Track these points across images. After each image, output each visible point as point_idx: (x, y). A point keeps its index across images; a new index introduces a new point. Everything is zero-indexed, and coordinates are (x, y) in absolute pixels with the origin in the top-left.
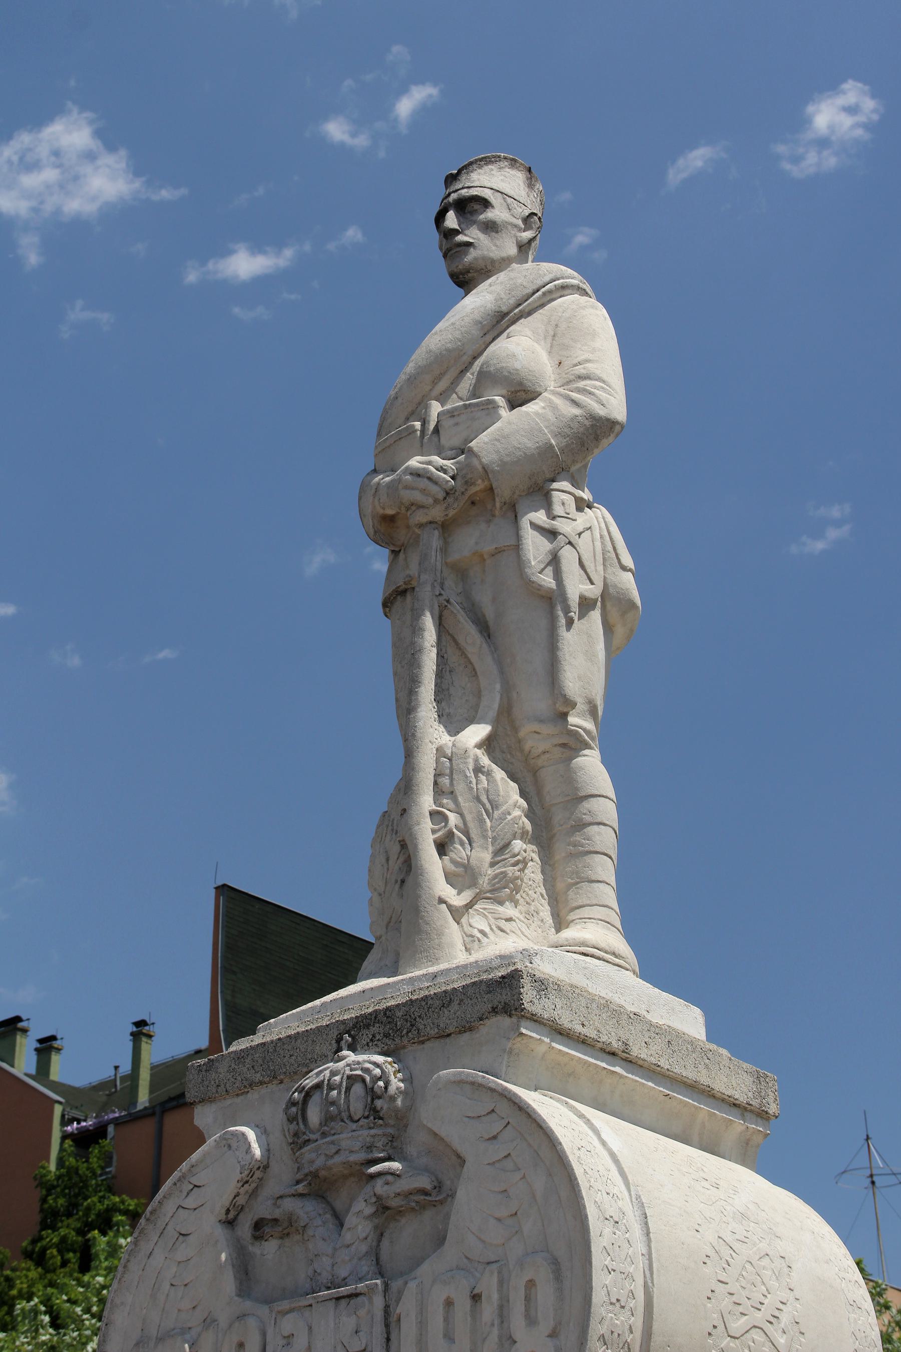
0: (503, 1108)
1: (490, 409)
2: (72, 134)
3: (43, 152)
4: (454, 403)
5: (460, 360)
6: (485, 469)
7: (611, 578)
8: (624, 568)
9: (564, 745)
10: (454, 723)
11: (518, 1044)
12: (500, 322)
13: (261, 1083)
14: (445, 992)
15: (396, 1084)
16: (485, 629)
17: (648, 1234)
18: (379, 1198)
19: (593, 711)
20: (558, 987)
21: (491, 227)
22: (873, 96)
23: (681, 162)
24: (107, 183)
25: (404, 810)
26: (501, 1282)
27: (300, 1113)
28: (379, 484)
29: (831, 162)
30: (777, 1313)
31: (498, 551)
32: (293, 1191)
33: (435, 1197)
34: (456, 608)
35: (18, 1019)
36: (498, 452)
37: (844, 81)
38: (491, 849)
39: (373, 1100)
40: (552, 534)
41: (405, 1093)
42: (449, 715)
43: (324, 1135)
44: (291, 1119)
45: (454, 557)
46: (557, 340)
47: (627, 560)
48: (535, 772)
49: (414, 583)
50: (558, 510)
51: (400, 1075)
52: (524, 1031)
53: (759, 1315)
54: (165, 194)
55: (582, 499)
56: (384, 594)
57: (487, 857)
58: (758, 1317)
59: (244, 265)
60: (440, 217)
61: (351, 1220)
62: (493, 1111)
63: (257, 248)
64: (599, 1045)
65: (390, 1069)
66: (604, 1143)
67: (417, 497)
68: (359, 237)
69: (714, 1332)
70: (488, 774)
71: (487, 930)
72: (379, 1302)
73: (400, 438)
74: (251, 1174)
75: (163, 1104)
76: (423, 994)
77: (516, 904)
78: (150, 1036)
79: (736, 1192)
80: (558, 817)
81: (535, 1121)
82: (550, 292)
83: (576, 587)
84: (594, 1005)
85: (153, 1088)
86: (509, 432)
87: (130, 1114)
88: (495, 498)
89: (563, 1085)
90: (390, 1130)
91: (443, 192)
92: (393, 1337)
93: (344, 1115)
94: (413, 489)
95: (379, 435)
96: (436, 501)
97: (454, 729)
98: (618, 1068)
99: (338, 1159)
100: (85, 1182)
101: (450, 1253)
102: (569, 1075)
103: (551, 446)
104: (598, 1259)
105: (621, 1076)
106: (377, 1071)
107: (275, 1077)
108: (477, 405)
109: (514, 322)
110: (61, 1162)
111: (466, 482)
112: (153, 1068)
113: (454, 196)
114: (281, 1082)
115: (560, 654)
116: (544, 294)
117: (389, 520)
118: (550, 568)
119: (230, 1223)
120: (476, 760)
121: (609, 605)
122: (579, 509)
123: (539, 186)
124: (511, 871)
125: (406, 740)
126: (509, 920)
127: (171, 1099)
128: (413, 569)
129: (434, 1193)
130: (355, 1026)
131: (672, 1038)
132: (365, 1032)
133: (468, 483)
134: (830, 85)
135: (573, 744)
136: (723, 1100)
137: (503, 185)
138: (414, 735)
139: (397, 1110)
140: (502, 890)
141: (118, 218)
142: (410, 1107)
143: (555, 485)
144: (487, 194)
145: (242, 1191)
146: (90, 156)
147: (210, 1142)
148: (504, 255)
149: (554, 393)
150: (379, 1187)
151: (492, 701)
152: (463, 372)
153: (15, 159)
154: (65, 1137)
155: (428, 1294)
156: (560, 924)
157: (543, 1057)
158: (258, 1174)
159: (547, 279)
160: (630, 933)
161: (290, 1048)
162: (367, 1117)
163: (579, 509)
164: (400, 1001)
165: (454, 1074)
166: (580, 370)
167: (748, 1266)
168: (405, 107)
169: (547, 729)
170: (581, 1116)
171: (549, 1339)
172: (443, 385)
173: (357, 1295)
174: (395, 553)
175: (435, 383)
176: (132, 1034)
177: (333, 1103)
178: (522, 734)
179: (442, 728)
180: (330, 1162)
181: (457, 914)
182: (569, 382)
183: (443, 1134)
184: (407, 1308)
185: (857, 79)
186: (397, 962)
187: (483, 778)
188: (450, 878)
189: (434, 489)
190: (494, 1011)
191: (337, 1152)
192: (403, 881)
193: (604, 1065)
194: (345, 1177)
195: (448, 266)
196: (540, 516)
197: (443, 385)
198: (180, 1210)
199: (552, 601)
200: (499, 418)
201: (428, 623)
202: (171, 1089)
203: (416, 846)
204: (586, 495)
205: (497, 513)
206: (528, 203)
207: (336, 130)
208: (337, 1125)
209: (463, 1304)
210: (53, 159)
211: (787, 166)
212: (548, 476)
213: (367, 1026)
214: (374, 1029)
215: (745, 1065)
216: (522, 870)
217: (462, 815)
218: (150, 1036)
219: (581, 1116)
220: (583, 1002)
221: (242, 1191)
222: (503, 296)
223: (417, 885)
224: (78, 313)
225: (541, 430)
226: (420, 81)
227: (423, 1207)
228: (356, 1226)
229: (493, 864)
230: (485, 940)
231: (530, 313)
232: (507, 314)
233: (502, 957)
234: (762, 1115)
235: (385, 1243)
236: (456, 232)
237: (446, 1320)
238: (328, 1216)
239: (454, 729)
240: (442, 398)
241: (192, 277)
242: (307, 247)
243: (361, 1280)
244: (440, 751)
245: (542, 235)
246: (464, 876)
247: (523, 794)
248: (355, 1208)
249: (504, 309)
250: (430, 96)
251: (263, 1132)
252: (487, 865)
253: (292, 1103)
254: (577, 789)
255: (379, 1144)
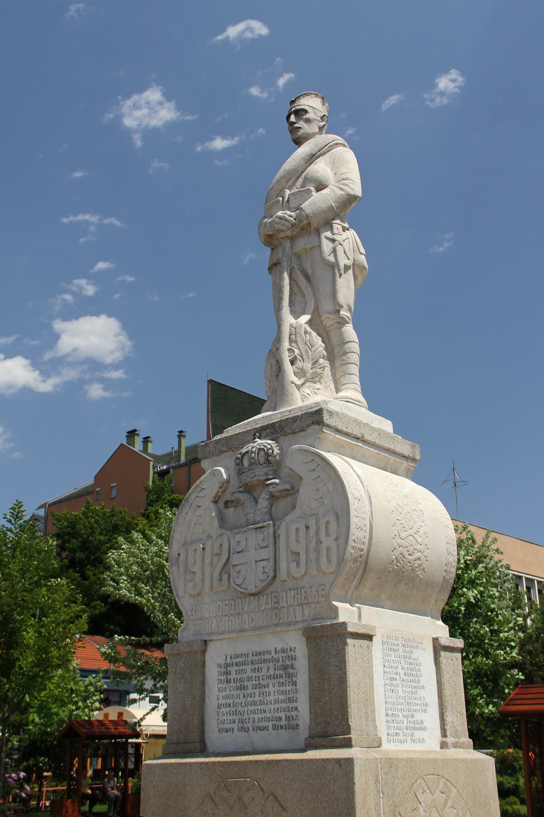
0: (317, 459)
1: (309, 192)
2: (154, 95)
3: (143, 102)
4: (295, 190)
5: (297, 173)
6: (307, 216)
7: (356, 258)
8: (361, 254)
9: (339, 322)
10: (296, 315)
11: (322, 435)
12: (312, 158)
13: (226, 451)
14: (294, 416)
15: (276, 451)
16: (308, 279)
17: (371, 503)
18: (271, 493)
19: (350, 309)
20: (337, 414)
21: (308, 121)
22: (462, 76)
23: (387, 101)
24: (167, 114)
25: (278, 348)
26: (317, 522)
28: (266, 222)
29: (445, 101)
30: (418, 530)
31: (313, 248)
32: (238, 490)
33: (292, 492)
34: (296, 270)
35: (135, 430)
36: (312, 209)
37: (451, 69)
38: (311, 363)
40: (333, 241)
41: (280, 454)
42: (294, 311)
43: (250, 470)
44: (237, 464)
45: (295, 250)
46: (334, 165)
47: (363, 251)
48: (328, 333)
49: (280, 261)
50: (335, 231)
51: (278, 448)
52: (324, 430)
53: (411, 531)
54: (189, 117)
55: (345, 227)
56: (269, 264)
57: (310, 365)
58: (411, 532)
59: (219, 144)
60: (288, 117)
61: (260, 501)
63: (224, 137)
64: (353, 435)
65: (274, 446)
66: (355, 471)
67: (281, 227)
68: (264, 132)
69: (395, 537)
70: (310, 334)
71: (310, 393)
72: (271, 529)
73: (274, 204)
74: (223, 484)
75: (190, 461)
76: (286, 417)
77: (321, 383)
78: (184, 437)
79: (404, 488)
80: (337, 350)
81: (329, 463)
82: (331, 146)
83: (343, 261)
84: (351, 421)
85: (186, 455)
86: (316, 202)
87: (178, 465)
88: (310, 227)
89: (339, 450)
90: (274, 468)
91: (289, 107)
92: (277, 542)
93: (257, 463)
94: (279, 224)
95: (266, 203)
96: (288, 229)
97: (296, 318)
98: (359, 443)
99: (255, 479)
100: (163, 489)
101: (297, 512)
102: (342, 447)
103: (333, 206)
104: (352, 513)
105: (361, 447)
106: (269, 446)
107: (231, 449)
108: (303, 190)
109: (317, 158)
110: (154, 482)
111: (300, 221)
112: (186, 448)
113: (294, 109)
114: (233, 451)
115: (337, 287)
116: (329, 147)
117: (270, 236)
118: (333, 254)
119: (215, 502)
120: (305, 329)
121: (355, 268)
122: (344, 231)
123: (327, 104)
124: (319, 371)
125: (278, 321)
126: (318, 389)
127: (193, 459)
128: (280, 255)
129: (291, 490)
130: (260, 430)
131: (380, 432)
132: (264, 432)
133: (301, 221)
134: (446, 71)
135: (342, 322)
136: (399, 455)
137: (313, 105)
138: (281, 320)
139: (277, 461)
140: (315, 378)
141: (170, 126)
142: (282, 459)
143: (334, 222)
144: (306, 108)
145: (220, 490)
146: (161, 103)
147: (207, 473)
148: (313, 131)
149: (333, 185)
150: (271, 488)
151: (311, 306)
152: (298, 178)
153: (132, 105)
154: (154, 473)
155: (290, 527)
156: (338, 390)
157: (332, 440)
158: (225, 484)
159: (330, 141)
160: (364, 393)
163: (344, 231)
164: (277, 420)
165: (298, 447)
166: (343, 176)
167: (408, 514)
168: (281, 82)
169: (332, 317)
170: (346, 461)
172: (290, 183)
173: (263, 527)
174: (273, 249)
175: (287, 182)
176: (178, 436)
177: (253, 458)
178: (322, 318)
179: (292, 317)
180: (253, 480)
181: (298, 387)
182: (339, 181)
183: (294, 469)
184: (282, 531)
185: (455, 68)
186: (276, 406)
187: (308, 335)
188: (295, 374)
189: (287, 224)
190: (313, 423)
191: (255, 476)
192: (278, 375)
193: (355, 443)
194: (258, 485)
195: (292, 136)
196: (328, 234)
197: (290, 183)
199: (333, 267)
200: (312, 195)
201: (286, 276)
202: (193, 456)
203: (282, 362)
204: (346, 225)
205: (312, 233)
206: (323, 111)
207: (255, 91)
208: (255, 466)
209: (303, 530)
210: (146, 105)
211: (429, 103)
212: (331, 218)
213: (265, 430)
214: (268, 431)
215: (408, 442)
216: (323, 370)
217: (300, 350)
218: (184, 437)
219: (346, 461)
220: (347, 419)
221: (220, 490)
222: (313, 147)
223: (283, 377)
224: (156, 164)
225: (328, 200)
226: (287, 72)
227: (287, 496)
229: (312, 368)
230: (309, 397)
231: (324, 154)
232: (315, 155)
233: (316, 403)
234: (414, 460)
235: (273, 508)
236: (295, 123)
237: (296, 535)
238: (252, 499)
239: (296, 318)
240: (290, 188)
241: (199, 149)
242: (244, 137)
243: (265, 522)
244: (291, 325)
245: (330, 125)
246: (300, 373)
247: (323, 341)
248: (262, 496)
249: (314, 153)
250: (291, 77)
251: (227, 469)
252: (310, 368)
253: (237, 459)
254: (344, 339)
255: (270, 473)
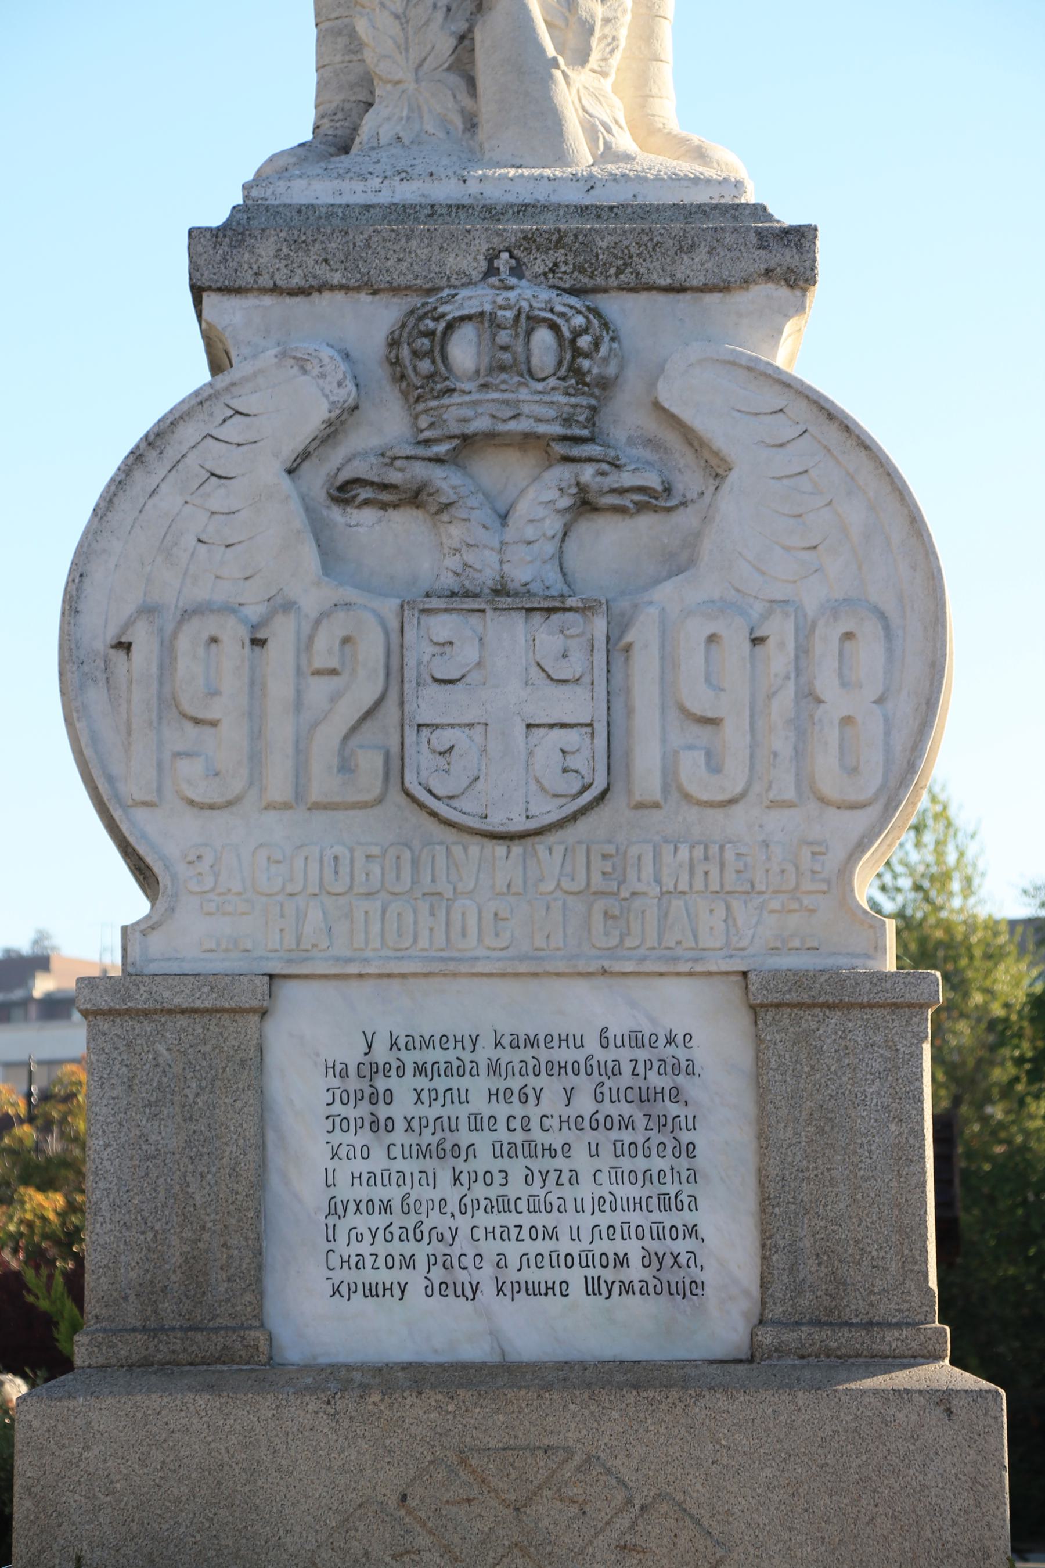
18: (582, 488)
27: (437, 349)
39: (574, 358)
62: (781, 410)
161: (397, 247)
162: (563, 379)
171: (874, 705)
190: (768, 274)
191: (514, 417)
198: (210, 440)
209: (736, 640)
227: (641, 508)
228: (543, 519)
255: (582, 418)
